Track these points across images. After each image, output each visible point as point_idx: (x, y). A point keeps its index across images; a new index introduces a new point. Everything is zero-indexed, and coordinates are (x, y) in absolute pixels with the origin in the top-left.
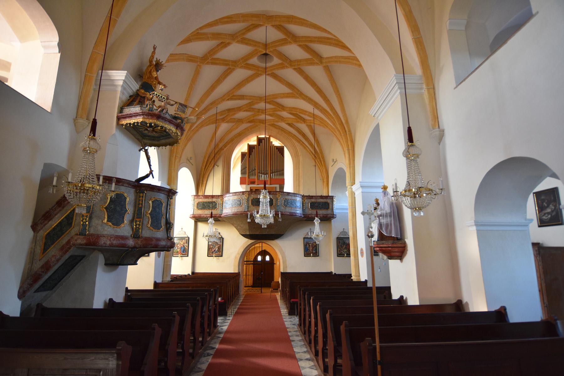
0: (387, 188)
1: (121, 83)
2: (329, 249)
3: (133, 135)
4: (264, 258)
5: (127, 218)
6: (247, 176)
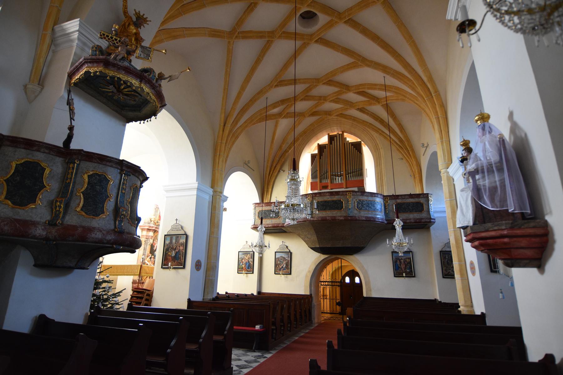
0: (489, 117)
1: (76, 35)
2: (428, 266)
3: (104, 103)
4: (352, 280)
5: (43, 198)
6: (318, 180)
